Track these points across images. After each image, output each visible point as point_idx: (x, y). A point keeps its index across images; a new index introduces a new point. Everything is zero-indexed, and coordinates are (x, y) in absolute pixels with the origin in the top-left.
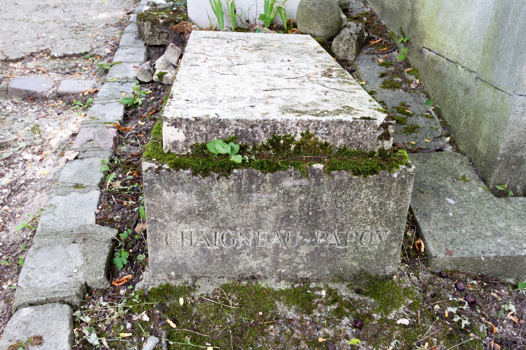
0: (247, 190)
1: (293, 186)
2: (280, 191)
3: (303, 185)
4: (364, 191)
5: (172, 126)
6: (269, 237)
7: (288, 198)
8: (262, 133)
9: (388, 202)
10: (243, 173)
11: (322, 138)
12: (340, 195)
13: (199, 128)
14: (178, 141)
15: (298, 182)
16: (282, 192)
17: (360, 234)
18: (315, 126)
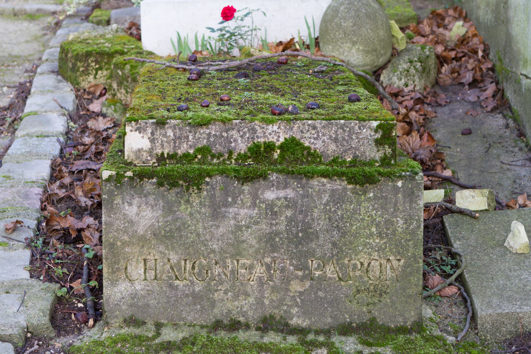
0: (221, 203)
1: (277, 199)
2: (261, 205)
3: (289, 196)
4: (363, 204)
5: (136, 131)
6: (251, 267)
7: (271, 215)
8: (240, 139)
9: (395, 220)
10: (217, 182)
11: (310, 143)
12: (335, 210)
13: (166, 133)
14: (142, 149)
15: (282, 194)
16: (264, 207)
17: (366, 265)
18: (301, 129)
